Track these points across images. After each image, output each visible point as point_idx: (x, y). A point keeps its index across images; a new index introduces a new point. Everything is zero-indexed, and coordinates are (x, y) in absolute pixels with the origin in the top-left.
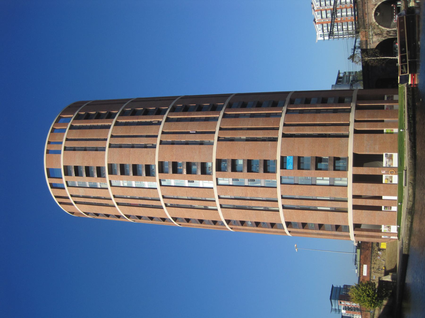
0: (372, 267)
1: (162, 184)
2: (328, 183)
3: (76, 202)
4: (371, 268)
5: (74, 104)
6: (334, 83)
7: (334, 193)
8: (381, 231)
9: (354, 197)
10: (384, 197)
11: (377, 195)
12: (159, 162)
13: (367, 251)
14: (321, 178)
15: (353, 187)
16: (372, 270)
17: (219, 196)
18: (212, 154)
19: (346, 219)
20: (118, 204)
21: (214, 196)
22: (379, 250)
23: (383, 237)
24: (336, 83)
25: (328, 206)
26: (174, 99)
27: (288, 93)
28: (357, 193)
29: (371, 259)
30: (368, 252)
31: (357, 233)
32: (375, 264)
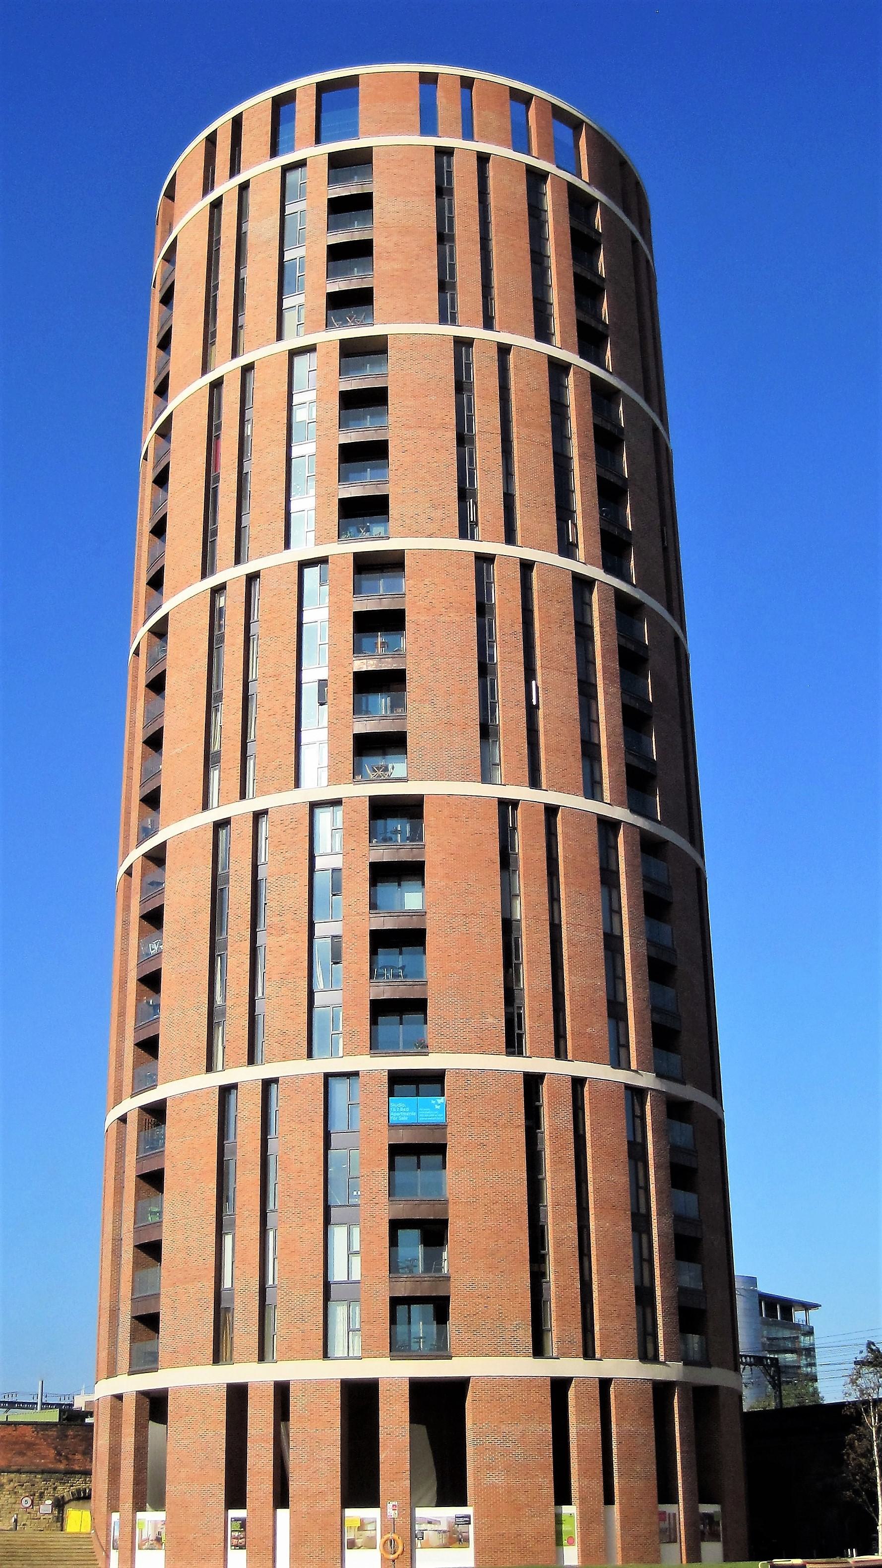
1: (307, 571)
5: (638, 184)
7: (295, 1301)
10: (283, 1515)
11: (294, 1487)
13: (52, 1453)
14: (356, 1247)
22: (60, 1505)
23: (115, 1516)
26: (670, 609)
29: (19, 1472)
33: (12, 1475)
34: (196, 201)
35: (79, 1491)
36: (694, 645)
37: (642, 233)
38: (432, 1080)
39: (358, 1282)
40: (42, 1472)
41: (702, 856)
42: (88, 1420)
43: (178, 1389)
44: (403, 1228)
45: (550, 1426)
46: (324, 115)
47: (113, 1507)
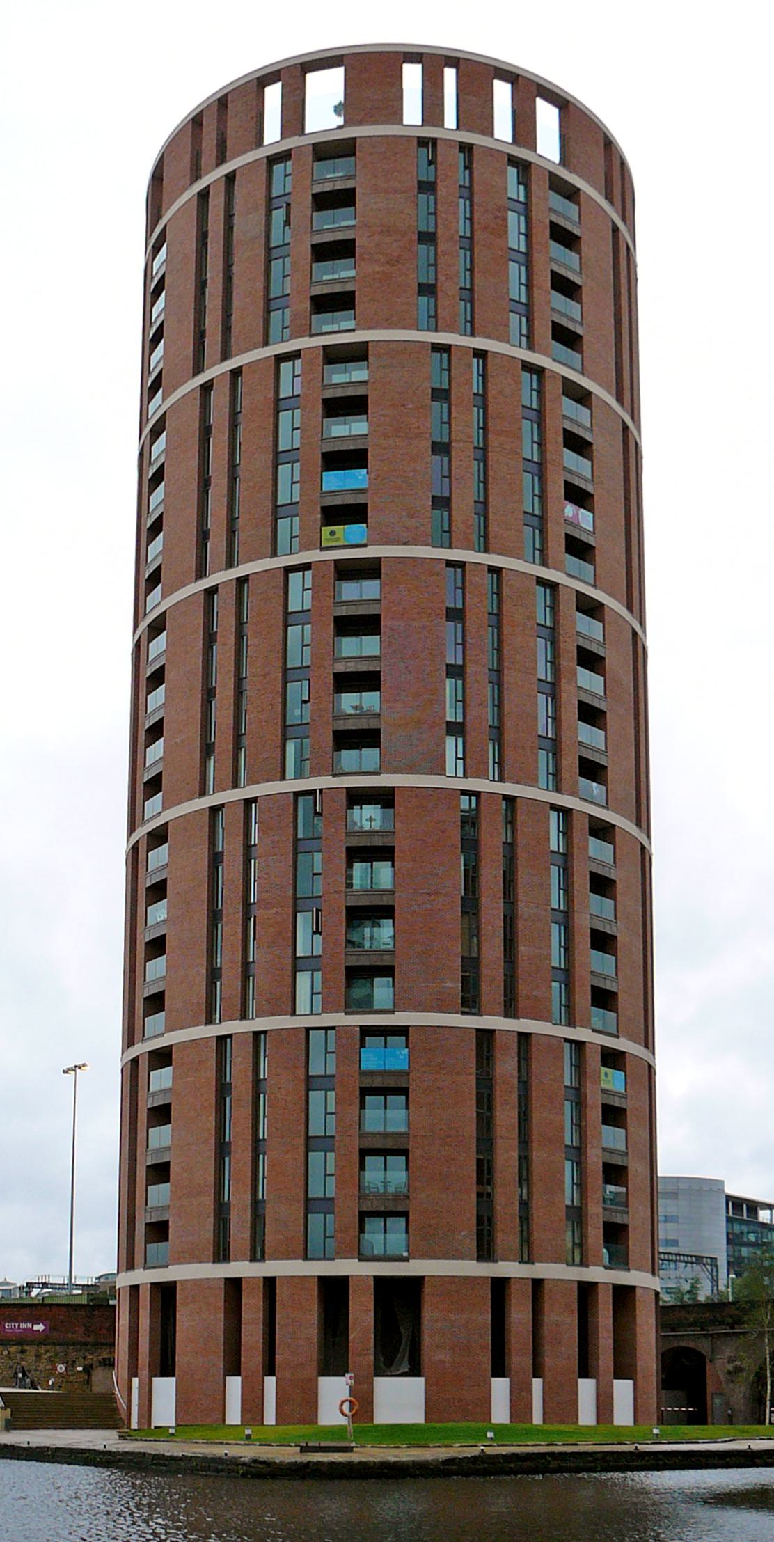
0: (26, 1348)
1: (300, 799)
2: (316, 1129)
3: (204, 195)
4: (19, 1343)
5: (623, 163)
6: (732, 1189)
7: (282, 1215)
8: (386, 1366)
9: (270, 1282)
10: (270, 1382)
11: (279, 1358)
12: (378, 560)
13: (82, 1330)
14: (331, 1108)
15: (304, 1278)
16: (13, 1349)
17: (254, 800)
18: (411, 770)
19: (190, 1256)
20: (207, 388)
21: (252, 781)
22: (88, 1369)
23: (135, 1381)
24: (729, 1198)
25: (238, 1200)
26: (630, 608)
27: (648, 1041)
28: (282, 1294)
29: (54, 1344)
30: (79, 1334)
31: (145, 1297)
32: (38, 1356)
33: (48, 1347)
34: (185, 189)
35: (104, 1359)
36: (653, 641)
37: (624, 219)
38: (369, 569)
39: (333, 1137)
40: (73, 1344)
41: (649, 836)
42: (111, 1302)
43: (181, 1281)
44: (370, 1095)
45: (489, 1291)
46: (347, 770)
47: (133, 1372)
